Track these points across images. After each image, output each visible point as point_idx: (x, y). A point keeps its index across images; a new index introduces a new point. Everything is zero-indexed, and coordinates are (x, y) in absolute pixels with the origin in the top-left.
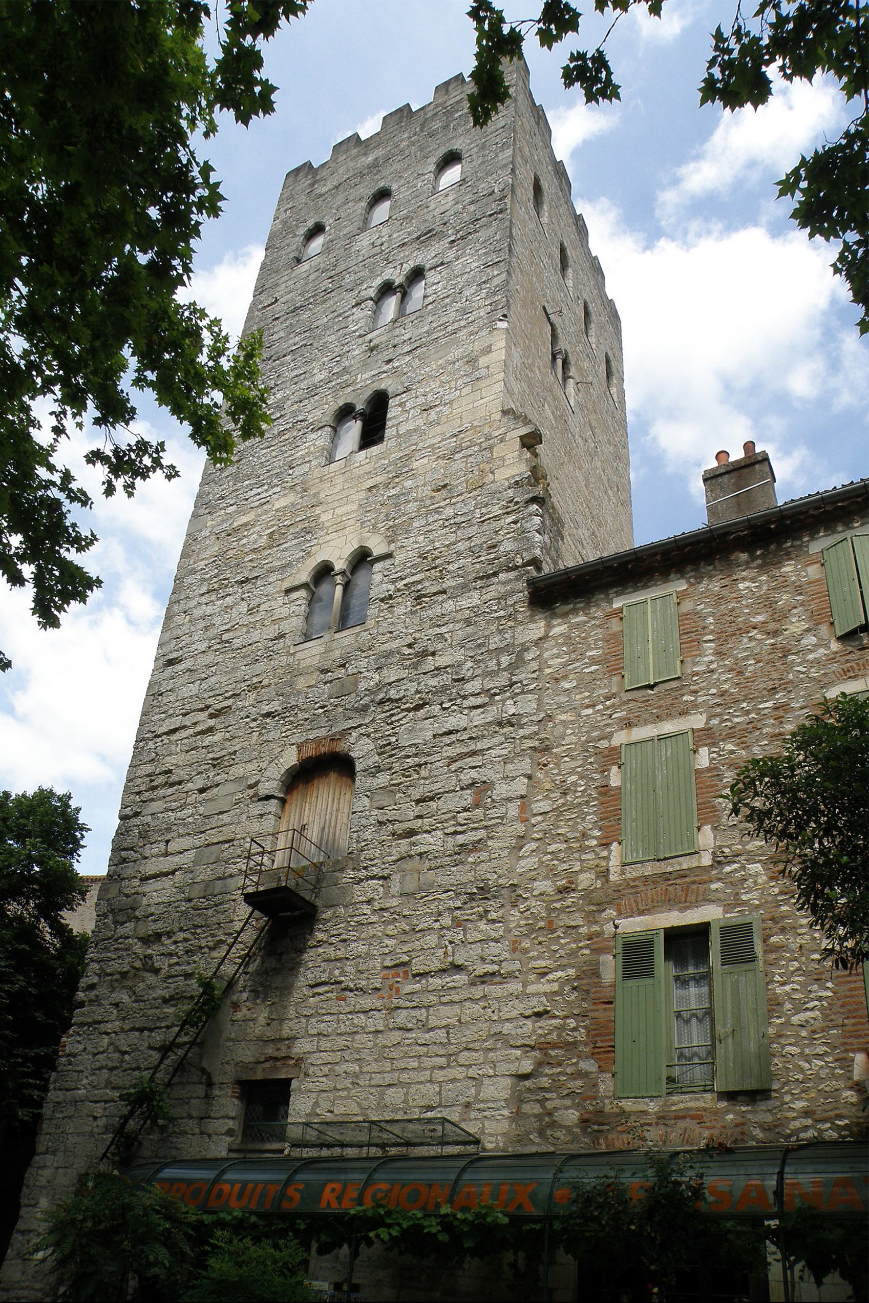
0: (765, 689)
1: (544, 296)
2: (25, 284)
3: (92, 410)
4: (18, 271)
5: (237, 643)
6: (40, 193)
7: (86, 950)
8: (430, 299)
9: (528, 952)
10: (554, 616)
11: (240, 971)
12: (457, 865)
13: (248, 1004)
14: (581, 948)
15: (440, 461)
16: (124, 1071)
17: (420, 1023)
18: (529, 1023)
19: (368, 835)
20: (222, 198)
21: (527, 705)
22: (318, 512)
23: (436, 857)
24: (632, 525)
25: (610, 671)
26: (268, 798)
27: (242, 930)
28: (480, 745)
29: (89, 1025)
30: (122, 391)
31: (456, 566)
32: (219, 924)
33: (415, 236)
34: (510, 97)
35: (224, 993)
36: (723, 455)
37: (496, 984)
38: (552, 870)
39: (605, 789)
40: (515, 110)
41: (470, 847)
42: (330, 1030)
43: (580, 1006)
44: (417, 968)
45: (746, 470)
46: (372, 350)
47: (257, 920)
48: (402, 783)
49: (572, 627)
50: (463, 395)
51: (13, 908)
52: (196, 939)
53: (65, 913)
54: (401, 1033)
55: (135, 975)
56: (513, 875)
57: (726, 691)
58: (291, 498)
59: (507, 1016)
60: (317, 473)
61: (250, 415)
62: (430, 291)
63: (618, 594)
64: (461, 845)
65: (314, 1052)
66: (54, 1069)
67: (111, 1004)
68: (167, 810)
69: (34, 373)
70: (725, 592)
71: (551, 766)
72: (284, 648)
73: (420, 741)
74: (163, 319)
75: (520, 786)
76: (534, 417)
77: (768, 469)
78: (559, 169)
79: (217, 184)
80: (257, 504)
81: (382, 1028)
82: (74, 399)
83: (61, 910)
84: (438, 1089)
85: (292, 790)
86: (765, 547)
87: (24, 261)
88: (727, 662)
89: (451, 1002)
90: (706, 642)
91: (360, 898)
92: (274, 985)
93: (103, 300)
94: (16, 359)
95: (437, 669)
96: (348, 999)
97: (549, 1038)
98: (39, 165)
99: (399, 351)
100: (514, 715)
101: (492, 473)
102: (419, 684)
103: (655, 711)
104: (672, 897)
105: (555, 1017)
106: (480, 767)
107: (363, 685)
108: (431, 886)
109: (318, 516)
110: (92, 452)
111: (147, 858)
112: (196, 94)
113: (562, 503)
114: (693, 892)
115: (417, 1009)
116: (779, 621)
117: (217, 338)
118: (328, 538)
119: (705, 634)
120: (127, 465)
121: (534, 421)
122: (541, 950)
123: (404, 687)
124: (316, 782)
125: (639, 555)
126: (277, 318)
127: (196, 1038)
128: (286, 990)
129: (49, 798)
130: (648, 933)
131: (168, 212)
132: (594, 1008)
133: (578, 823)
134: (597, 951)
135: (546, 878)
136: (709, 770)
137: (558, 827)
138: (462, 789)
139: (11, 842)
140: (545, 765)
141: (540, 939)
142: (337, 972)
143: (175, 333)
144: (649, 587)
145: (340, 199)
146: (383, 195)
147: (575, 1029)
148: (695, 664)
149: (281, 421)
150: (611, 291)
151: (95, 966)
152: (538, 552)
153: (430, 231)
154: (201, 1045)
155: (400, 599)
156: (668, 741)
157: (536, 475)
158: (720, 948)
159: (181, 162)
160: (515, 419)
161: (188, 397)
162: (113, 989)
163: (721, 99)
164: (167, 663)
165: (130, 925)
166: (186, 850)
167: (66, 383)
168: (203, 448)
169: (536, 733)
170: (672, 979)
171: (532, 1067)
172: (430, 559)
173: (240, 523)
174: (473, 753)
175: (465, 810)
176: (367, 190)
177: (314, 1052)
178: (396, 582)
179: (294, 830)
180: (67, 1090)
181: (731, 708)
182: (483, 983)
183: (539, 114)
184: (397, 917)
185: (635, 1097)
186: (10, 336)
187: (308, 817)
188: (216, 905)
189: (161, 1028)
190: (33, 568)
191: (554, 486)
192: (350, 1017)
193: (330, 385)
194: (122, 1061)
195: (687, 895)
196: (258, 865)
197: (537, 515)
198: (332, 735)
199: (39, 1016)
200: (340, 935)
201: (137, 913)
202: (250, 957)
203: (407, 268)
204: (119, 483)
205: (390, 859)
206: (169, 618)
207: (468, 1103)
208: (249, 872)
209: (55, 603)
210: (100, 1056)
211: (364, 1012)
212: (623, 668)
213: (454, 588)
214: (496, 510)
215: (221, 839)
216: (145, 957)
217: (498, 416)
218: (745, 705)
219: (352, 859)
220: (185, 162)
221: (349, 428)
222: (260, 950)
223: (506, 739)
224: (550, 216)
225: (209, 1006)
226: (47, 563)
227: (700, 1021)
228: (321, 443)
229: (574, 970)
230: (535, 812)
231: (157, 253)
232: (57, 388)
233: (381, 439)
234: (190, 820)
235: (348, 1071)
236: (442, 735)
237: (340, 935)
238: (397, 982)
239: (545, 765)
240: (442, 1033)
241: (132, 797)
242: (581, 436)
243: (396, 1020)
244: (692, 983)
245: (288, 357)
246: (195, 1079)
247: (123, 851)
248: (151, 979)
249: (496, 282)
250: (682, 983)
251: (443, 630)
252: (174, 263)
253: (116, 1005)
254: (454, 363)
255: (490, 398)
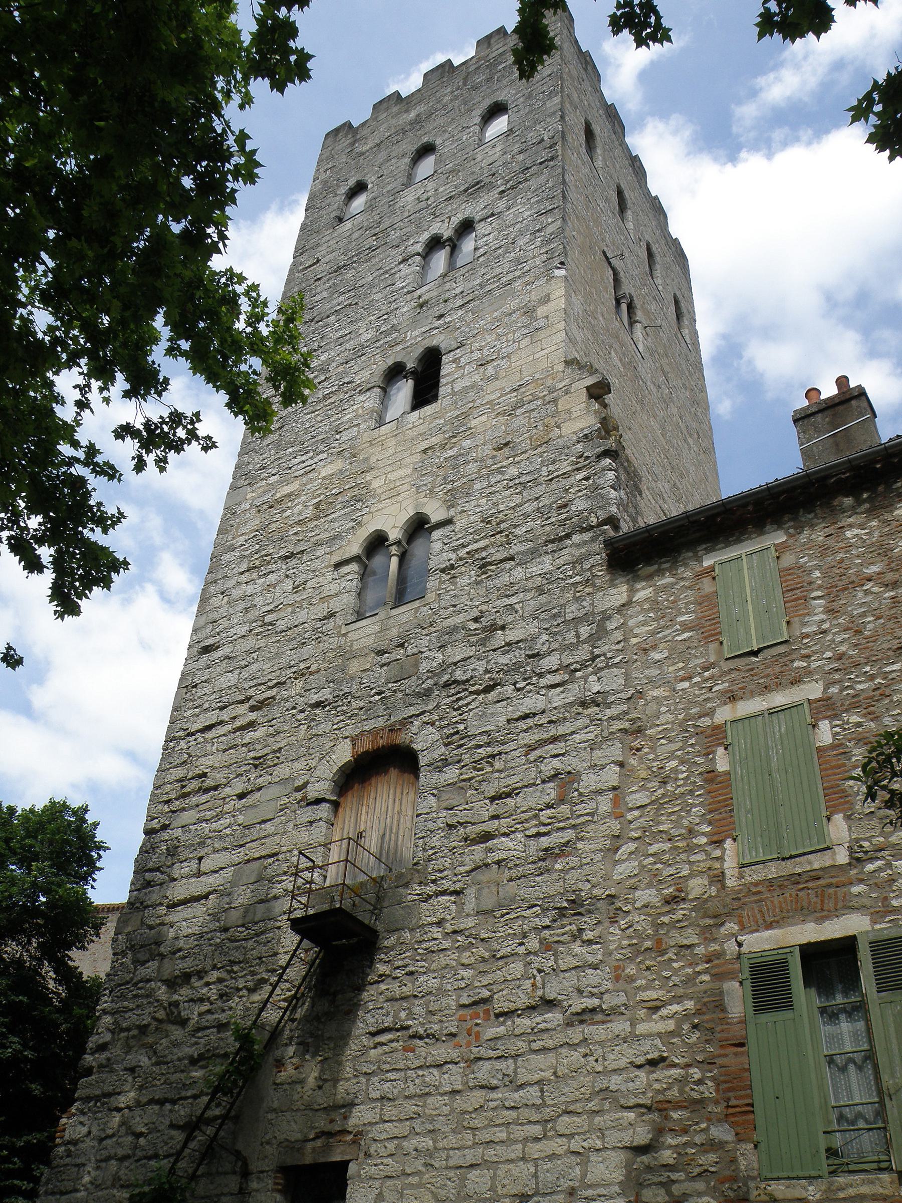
0: (889, 649)
1: (603, 240)
2: (52, 257)
3: (121, 383)
4: (45, 245)
5: (281, 625)
6: (68, 168)
7: (98, 999)
8: (482, 251)
9: (634, 981)
10: (637, 578)
11: (286, 1018)
12: (542, 874)
13: (294, 1060)
14: (699, 973)
15: (500, 418)
16: (137, 1161)
17: (507, 1079)
18: (642, 1074)
19: (435, 841)
20: (258, 165)
21: (613, 680)
22: (368, 478)
23: (516, 865)
24: (717, 474)
25: (706, 638)
26: (318, 801)
27: (288, 964)
28: (561, 730)
29: (97, 1098)
30: (153, 362)
31: (524, 529)
32: (260, 958)
33: (462, 188)
34: (556, 48)
35: (265, 1048)
36: (813, 393)
37: (597, 1023)
38: (655, 875)
39: (711, 775)
40: (561, 58)
41: (557, 851)
42: (396, 1091)
43: (704, 1051)
44: (501, 1004)
45: (841, 408)
46: (421, 306)
47: (306, 951)
48: (473, 778)
49: (658, 590)
50: (522, 346)
51: (12, 949)
52: (232, 978)
53: (74, 953)
54: (483, 1092)
55: (157, 1029)
56: (609, 883)
57: (843, 654)
58: (339, 464)
59: (614, 1066)
60: (366, 437)
61: (291, 382)
62: (481, 243)
63: (708, 551)
64: (546, 850)
65: (376, 1123)
66: (48, 1163)
67: (126, 1069)
68: (200, 821)
69: (59, 349)
70: (831, 542)
71: (646, 750)
72: (335, 628)
73: (493, 728)
74: (198, 288)
75: (612, 775)
76: (599, 365)
77: (866, 404)
78: (612, 113)
79: (254, 152)
80: (302, 472)
81: (460, 1087)
82: (102, 372)
83: (69, 949)
84: (532, 1170)
85: (346, 791)
86: (872, 489)
87: (51, 234)
88: (841, 621)
89: (544, 1050)
90: (814, 599)
91: (429, 919)
92: (327, 1035)
93: (133, 270)
94: (40, 335)
95: (508, 644)
96: (417, 1050)
97: (669, 1095)
98: (67, 141)
99: (450, 305)
100: (598, 692)
101: (558, 427)
102: (488, 662)
103: (762, 681)
104: (805, 904)
105: (674, 1066)
106: (563, 755)
107: (424, 667)
108: (513, 900)
109: (369, 483)
110: (121, 427)
111: (175, 880)
112: (232, 68)
113: (637, 456)
114: (830, 897)
115: (502, 1060)
116: (897, 570)
117: (254, 303)
118: (380, 505)
119: (813, 590)
120: (160, 440)
121: (601, 370)
122: (651, 978)
123: (472, 667)
124: (373, 781)
125: (728, 507)
126: (319, 279)
127: (229, 1111)
128: (343, 1039)
129: (61, 812)
130: (780, 951)
131: (202, 180)
132: (722, 1052)
133: (683, 817)
134: (719, 977)
135: (650, 885)
136: (832, 747)
137: (659, 823)
138: (544, 782)
139: (14, 867)
140: (638, 750)
141: (648, 963)
142: (403, 1014)
143: (210, 301)
144: (742, 541)
145: (382, 156)
146: (427, 149)
147: (700, 1082)
148: (804, 624)
149: (326, 384)
150: (676, 229)
151: (107, 1019)
152: (614, 509)
153: (478, 183)
154: (237, 1119)
155: (463, 569)
156: (781, 715)
157: (607, 427)
158: (872, 970)
159: (215, 131)
160: (580, 369)
161: (224, 365)
162: (128, 1049)
163: (779, 32)
164: (202, 649)
165: (153, 965)
166: (221, 869)
167: (92, 355)
168: (241, 417)
169: (626, 713)
170: (816, 1011)
171: (650, 1136)
172: (494, 523)
173: (283, 493)
174: (554, 739)
175: (549, 806)
176: (410, 146)
177: (376, 1123)
178: (457, 550)
179: (350, 839)
180: (62, 1193)
181: (851, 673)
182: (582, 1022)
183: (586, 61)
184: (474, 941)
185: (789, 1178)
186: (34, 310)
187: (366, 822)
188: (257, 935)
189: (186, 1098)
190: (52, 551)
191: (628, 438)
192: (420, 1073)
193: (378, 344)
194: (136, 1148)
195: (822, 902)
196: (307, 882)
197: (611, 470)
198: (392, 725)
199: (36, 1089)
200: (406, 966)
201: (162, 949)
202: (298, 999)
203: (456, 221)
204: (150, 459)
205: (462, 869)
206: (204, 599)
207: (573, 1188)
208: (296, 892)
209: (76, 588)
210: (109, 1142)
211: (438, 1066)
212: (720, 633)
213: (522, 553)
214: (565, 467)
215: (263, 853)
216: (170, 1004)
217: (561, 367)
218: (868, 669)
219: (418, 871)
220: (219, 131)
221: (399, 389)
222: (310, 990)
223: (591, 721)
224: (604, 160)
225: (248, 1061)
226: (68, 547)
227: (860, 1068)
228: (369, 404)
229: (692, 1003)
230: (630, 805)
231: (191, 223)
232: (83, 361)
233: (435, 398)
234: (228, 831)
235: (420, 1147)
236: (517, 720)
237: (406, 966)
238: (477, 1025)
239: (638, 750)
240: (534, 1091)
241: (160, 807)
242: (653, 383)
243: (477, 1075)
244: (842, 1017)
245: (332, 318)
246: (228, 1167)
247: (149, 873)
248: (177, 1033)
249: (550, 229)
250: (831, 1017)
251: (513, 600)
252: (209, 231)
253: (132, 1070)
254: (510, 314)
255: (552, 348)
